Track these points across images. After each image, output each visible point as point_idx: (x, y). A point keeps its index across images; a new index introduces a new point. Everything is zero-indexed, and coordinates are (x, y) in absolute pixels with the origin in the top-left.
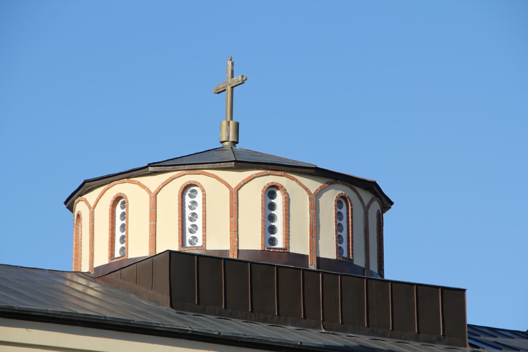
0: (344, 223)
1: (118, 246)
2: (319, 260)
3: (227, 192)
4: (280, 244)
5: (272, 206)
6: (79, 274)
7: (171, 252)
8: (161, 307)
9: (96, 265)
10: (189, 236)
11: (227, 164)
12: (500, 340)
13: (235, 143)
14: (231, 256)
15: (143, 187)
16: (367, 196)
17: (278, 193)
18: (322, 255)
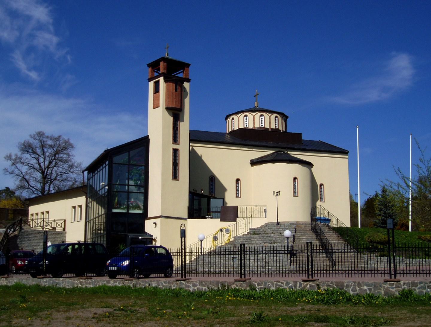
1: (233, 127)
6: (227, 133)
9: (229, 131)
11: (280, 126)
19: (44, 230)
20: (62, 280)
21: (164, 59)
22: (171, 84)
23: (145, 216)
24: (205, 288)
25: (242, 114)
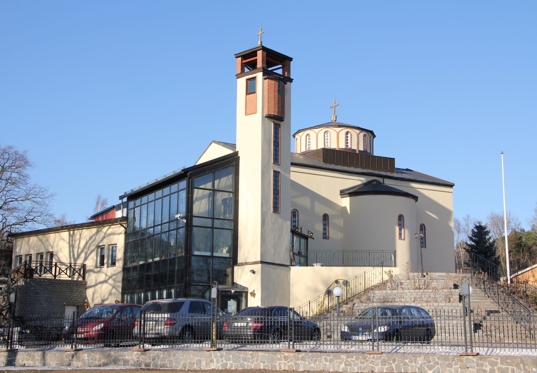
0: (365, 141)
2: (359, 151)
3: (315, 134)
4: (349, 147)
5: (347, 137)
6: (297, 153)
7: (323, 148)
8: (320, 162)
9: (302, 151)
10: (326, 144)
12: (401, 171)
13: (335, 121)
14: (337, 149)
15: (314, 132)
16: (370, 134)
17: (349, 133)
18: (360, 149)
19: (57, 278)
20: (251, 354)
21: (264, 49)
22: (273, 82)
23: (233, 260)
24: (513, 367)
25: (344, 129)
